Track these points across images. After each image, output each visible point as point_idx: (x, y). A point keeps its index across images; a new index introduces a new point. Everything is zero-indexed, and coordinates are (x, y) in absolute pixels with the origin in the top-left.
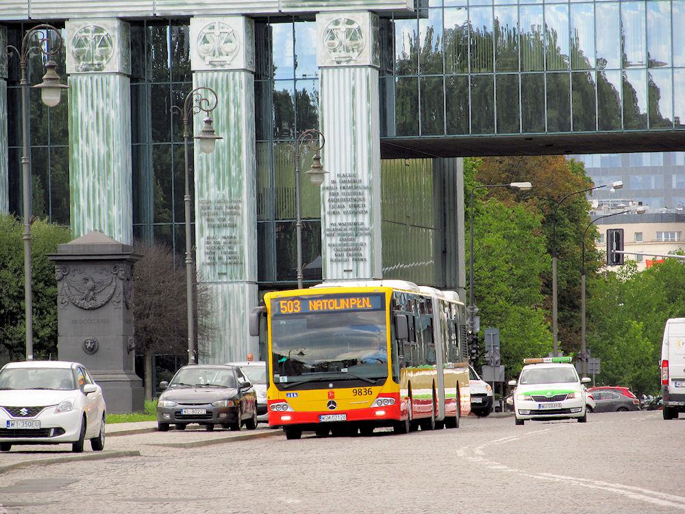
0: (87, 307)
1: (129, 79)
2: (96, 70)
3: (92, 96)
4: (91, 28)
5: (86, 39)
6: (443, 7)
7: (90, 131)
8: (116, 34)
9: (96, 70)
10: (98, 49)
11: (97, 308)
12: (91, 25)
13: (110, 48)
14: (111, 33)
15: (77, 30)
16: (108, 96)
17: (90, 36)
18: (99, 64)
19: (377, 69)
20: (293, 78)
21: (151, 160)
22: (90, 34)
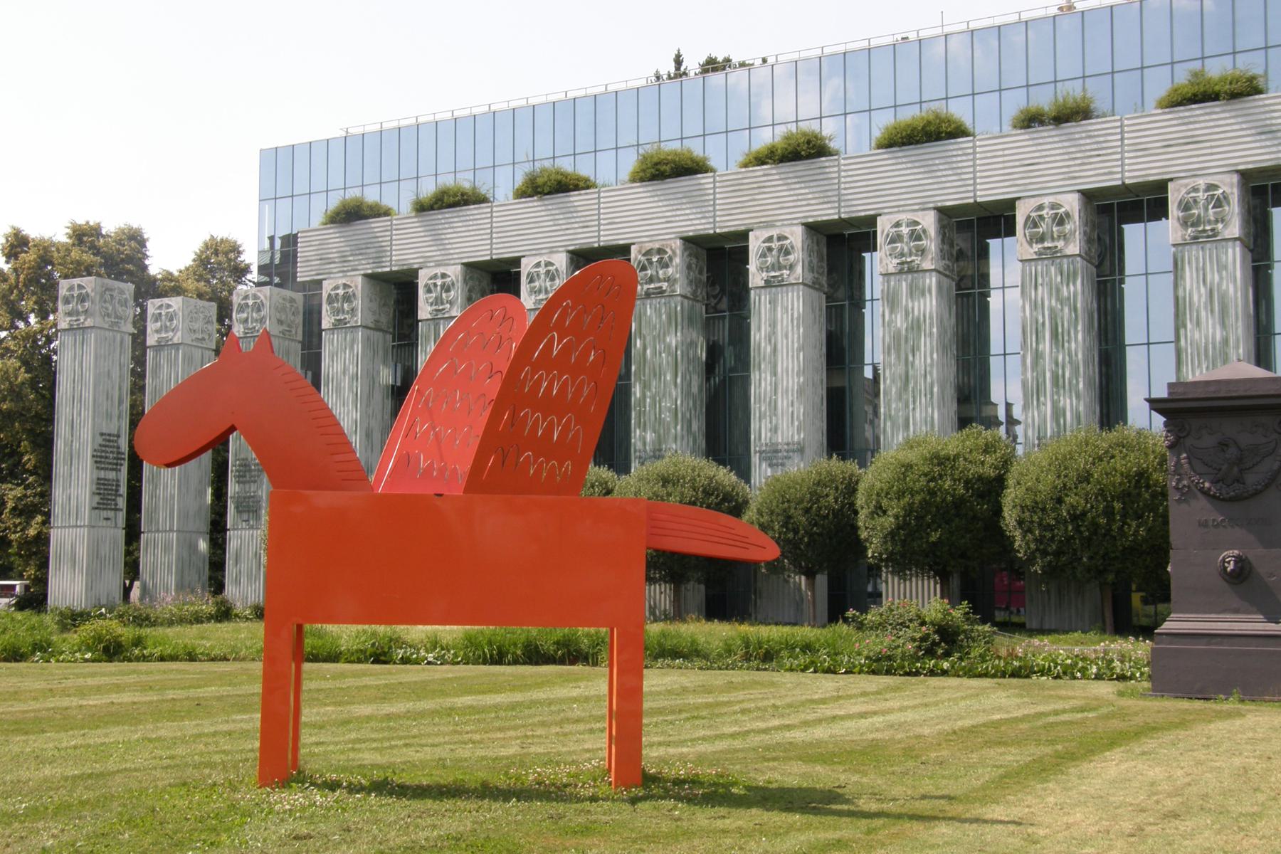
0: (1227, 496)
1: (824, 296)
2: (1209, 237)
3: (1204, 269)
4: (1203, 187)
5: (1195, 201)
6: (1005, 354)
7: (1203, 314)
8: (1235, 191)
9: (1209, 237)
10: (1211, 211)
11: (1246, 498)
12: (1201, 182)
13: (1227, 208)
14: (1228, 190)
15: (1184, 191)
16: (1226, 268)
17: (1201, 196)
18: (1212, 230)
19: (272, 258)
20: (1231, 57)
21: (667, 680)
22: (1200, 194)
